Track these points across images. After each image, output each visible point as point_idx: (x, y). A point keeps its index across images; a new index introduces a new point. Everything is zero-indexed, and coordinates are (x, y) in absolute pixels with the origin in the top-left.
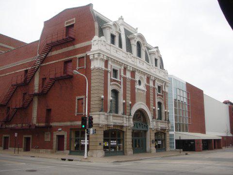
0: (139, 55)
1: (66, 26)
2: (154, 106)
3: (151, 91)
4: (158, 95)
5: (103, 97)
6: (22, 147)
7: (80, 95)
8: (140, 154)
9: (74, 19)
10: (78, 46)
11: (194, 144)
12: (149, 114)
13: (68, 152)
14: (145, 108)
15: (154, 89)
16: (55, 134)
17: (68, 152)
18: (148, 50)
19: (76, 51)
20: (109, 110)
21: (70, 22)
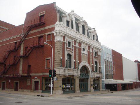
0: (84, 33)
1: (39, 15)
2: (93, 63)
3: (91, 55)
4: (95, 57)
6: (13, 88)
7: (48, 57)
8: (84, 92)
9: (45, 11)
10: (47, 28)
11: (117, 86)
12: (89, 69)
13: (41, 91)
14: (87, 65)
15: (93, 53)
16: (33, 80)
17: (41, 91)
18: (89, 30)
20: (65, 66)
21: (42, 13)
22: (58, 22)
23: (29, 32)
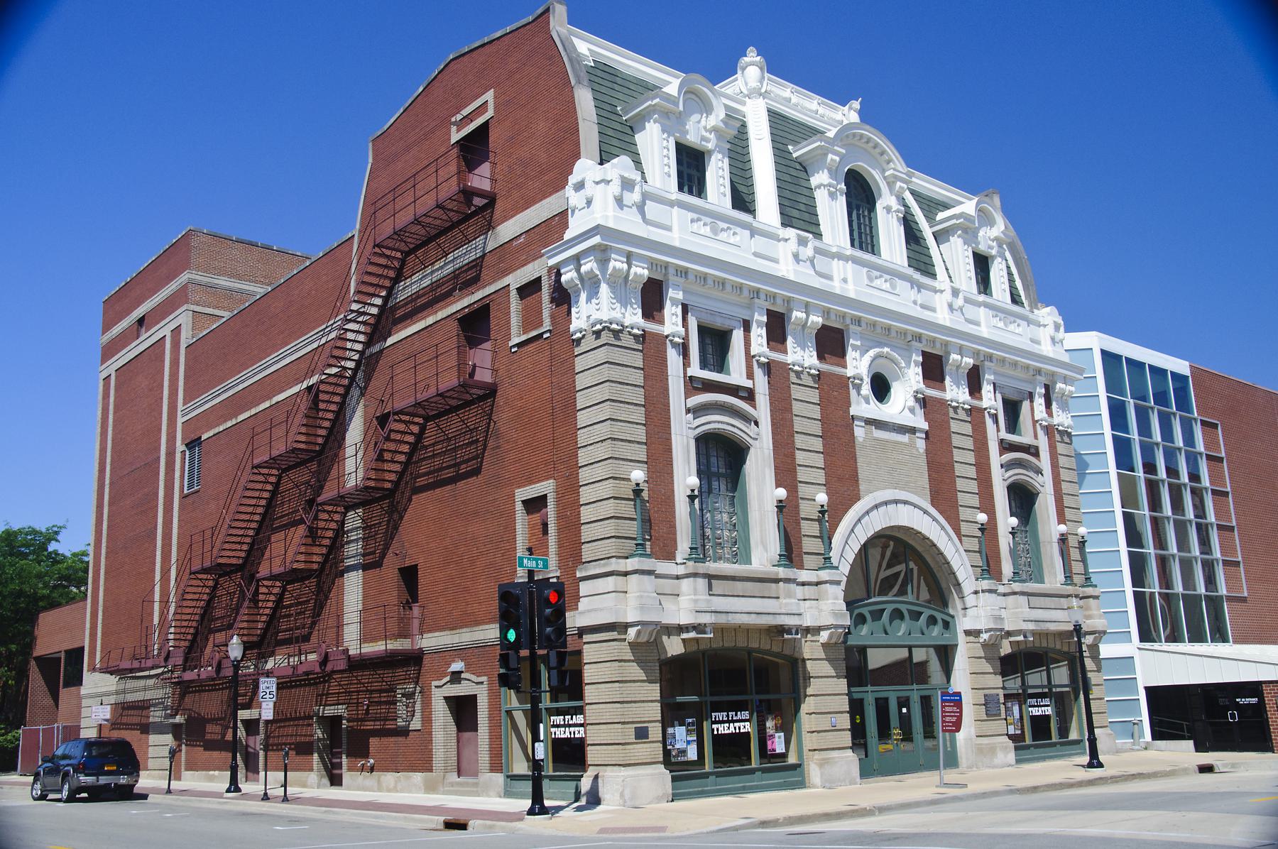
0: (864, 236)
1: (455, 136)
2: (987, 504)
3: (960, 429)
4: (1006, 447)
5: (638, 475)
6: (312, 770)
7: (531, 481)
8: (1088, 788)
9: (489, 96)
10: (508, 230)
11: (1260, 708)
12: (955, 564)
13: (499, 778)
14: (931, 527)
15: (976, 415)
16: (441, 692)
17: (499, 778)
18: (930, 218)
19: (513, 254)
20: (683, 545)
21: (469, 118)
22: (585, 168)
23: (390, 291)
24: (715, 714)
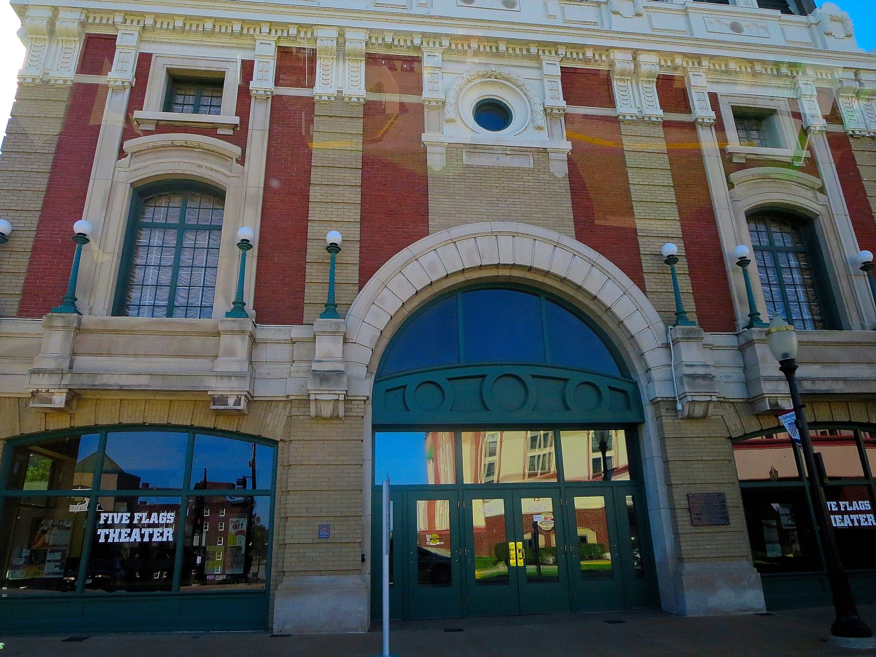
24: (140, 514)
